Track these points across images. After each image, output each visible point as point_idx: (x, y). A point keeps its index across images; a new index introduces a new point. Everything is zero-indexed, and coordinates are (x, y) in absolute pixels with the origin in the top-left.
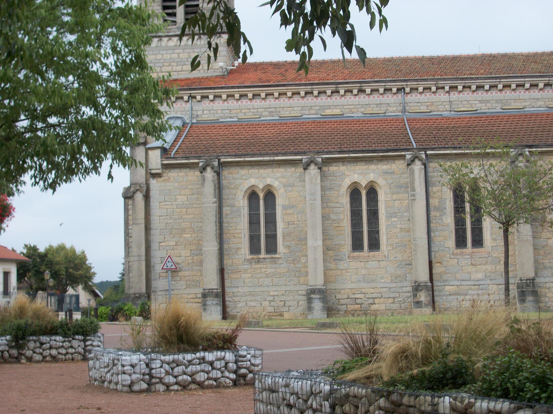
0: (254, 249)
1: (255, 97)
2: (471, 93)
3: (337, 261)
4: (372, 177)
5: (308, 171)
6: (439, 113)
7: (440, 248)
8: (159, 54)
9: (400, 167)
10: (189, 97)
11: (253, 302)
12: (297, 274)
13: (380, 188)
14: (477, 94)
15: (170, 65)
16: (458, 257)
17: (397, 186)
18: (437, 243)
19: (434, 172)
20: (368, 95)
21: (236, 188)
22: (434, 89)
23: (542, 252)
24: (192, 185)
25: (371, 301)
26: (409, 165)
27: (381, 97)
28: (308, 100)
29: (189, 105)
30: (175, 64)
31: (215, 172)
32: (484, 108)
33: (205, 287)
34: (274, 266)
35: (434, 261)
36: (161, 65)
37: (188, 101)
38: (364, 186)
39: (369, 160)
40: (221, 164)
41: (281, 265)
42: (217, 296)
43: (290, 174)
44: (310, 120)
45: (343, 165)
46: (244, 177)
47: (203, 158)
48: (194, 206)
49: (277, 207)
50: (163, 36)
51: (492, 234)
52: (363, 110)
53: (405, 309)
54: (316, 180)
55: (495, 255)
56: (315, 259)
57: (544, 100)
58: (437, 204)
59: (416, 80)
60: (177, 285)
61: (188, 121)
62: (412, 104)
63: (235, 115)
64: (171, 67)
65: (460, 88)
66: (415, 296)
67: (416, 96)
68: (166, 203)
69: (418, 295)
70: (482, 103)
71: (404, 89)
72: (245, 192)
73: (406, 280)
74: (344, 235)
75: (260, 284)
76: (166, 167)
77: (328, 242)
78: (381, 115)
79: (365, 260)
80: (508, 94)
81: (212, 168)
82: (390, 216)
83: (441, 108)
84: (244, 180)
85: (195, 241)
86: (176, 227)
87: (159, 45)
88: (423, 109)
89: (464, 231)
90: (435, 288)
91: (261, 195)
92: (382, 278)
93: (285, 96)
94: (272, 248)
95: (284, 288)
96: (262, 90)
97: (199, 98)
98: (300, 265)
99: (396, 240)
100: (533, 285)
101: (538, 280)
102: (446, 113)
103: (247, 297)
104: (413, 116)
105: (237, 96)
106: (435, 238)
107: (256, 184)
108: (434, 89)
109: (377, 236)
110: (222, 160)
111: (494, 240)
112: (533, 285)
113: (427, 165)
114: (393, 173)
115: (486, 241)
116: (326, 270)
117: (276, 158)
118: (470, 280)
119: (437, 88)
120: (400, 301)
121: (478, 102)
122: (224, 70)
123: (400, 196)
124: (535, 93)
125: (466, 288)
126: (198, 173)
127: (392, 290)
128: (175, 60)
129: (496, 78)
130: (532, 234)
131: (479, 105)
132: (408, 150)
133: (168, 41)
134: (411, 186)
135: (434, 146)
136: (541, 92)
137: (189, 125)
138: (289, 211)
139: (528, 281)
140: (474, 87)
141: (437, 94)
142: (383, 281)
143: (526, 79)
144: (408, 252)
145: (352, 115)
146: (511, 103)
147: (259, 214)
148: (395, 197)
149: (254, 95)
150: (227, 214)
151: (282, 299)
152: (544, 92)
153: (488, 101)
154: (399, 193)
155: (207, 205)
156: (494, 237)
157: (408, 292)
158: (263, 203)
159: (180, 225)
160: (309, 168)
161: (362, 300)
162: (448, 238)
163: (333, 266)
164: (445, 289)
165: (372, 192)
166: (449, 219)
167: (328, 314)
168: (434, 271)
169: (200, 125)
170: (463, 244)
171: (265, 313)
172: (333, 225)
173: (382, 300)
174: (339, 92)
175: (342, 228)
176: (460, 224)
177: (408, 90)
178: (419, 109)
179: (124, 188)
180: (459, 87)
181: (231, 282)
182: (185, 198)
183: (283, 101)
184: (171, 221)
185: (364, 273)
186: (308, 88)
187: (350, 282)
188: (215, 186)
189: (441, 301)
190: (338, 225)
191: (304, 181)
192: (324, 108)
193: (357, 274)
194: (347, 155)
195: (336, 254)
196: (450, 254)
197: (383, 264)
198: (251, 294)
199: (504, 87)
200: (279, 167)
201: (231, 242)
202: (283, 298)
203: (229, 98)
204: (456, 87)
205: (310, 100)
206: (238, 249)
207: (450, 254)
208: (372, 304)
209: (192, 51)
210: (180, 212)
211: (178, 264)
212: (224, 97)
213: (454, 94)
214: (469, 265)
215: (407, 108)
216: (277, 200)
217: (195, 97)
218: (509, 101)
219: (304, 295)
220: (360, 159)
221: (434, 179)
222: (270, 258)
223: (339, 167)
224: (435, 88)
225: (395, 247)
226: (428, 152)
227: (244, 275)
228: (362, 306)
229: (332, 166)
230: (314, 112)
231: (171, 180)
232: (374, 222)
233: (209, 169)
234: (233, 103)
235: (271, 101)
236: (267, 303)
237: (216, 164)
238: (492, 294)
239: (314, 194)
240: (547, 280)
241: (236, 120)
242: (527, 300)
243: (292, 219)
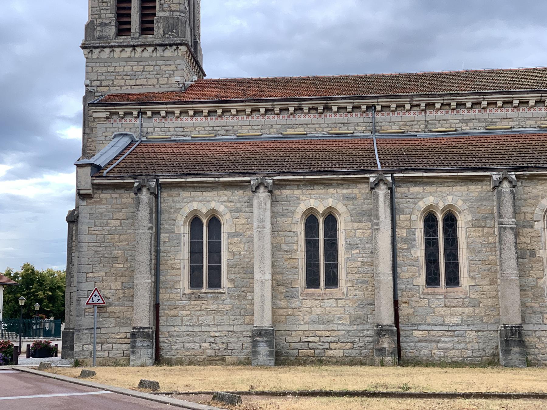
0: (195, 283)
1: (211, 114)
2: (450, 112)
3: (288, 298)
4: (330, 202)
5: (256, 194)
6: (413, 134)
7: (408, 286)
8: (111, 66)
9: (363, 191)
10: (139, 113)
11: (190, 344)
12: (242, 312)
13: (340, 215)
14: (458, 112)
15: (122, 79)
16: (429, 297)
17: (359, 213)
18: (405, 280)
19: (402, 198)
20: (334, 113)
21: (177, 212)
22: (408, 106)
23: (530, 294)
24: (127, 208)
25: (327, 346)
26: (372, 189)
27: (349, 115)
28: (268, 118)
29: (138, 121)
30: (129, 77)
31: (151, 194)
32: (464, 128)
33: (134, 325)
34: (215, 302)
35: (400, 300)
36: (113, 78)
37: (138, 117)
38: (321, 212)
39: (327, 184)
40: (159, 185)
41: (225, 302)
42: (147, 336)
43: (237, 198)
44: (270, 140)
45: (298, 189)
46: (185, 200)
47: (140, 177)
48: (128, 232)
49: (222, 235)
50: (115, 46)
51: (469, 271)
52: (327, 129)
53: (366, 356)
54: (266, 205)
55: (473, 296)
56: (262, 295)
57: (535, 119)
58: (405, 235)
59: (388, 97)
60: (104, 322)
61: (137, 139)
62: (383, 124)
63: (189, 133)
64: (124, 81)
65: (438, 105)
67: (388, 114)
68: (97, 228)
69: (380, 341)
70: (462, 123)
71: (375, 107)
72: (187, 217)
73: (367, 322)
74: (296, 268)
75: (200, 322)
76: (97, 187)
77: (279, 277)
78: (348, 135)
79: (320, 298)
80: (493, 113)
81: (148, 189)
82: (350, 247)
83: (416, 128)
84: (187, 204)
85: (127, 272)
86: (106, 255)
87: (112, 56)
88: (396, 129)
89: (437, 266)
90: (401, 333)
91: (205, 221)
92: (340, 319)
93: (243, 113)
94: (215, 282)
95: (227, 328)
96: (219, 107)
97: (149, 113)
98: (246, 302)
99: (357, 276)
100: (520, 333)
101: (525, 327)
102: (421, 133)
103: (185, 338)
104: (385, 137)
105: (191, 112)
106: (401, 275)
107: (199, 208)
108: (408, 106)
109: (335, 270)
110: (161, 180)
111: (473, 278)
112: (520, 333)
113: (394, 190)
114: (354, 198)
115: (462, 279)
116: (275, 308)
117: (222, 179)
118: (442, 325)
119: (412, 106)
120: (360, 347)
121: (458, 121)
122: (181, 85)
123: (362, 225)
124: (524, 112)
125: (438, 334)
126: (133, 195)
127: (351, 334)
128: (129, 73)
129: (480, 94)
130: (518, 272)
131: (460, 125)
132: (371, 172)
133: (121, 52)
134: (372, 215)
135: (402, 168)
136: (532, 110)
137: (137, 143)
138: (235, 240)
139: (514, 328)
140: (454, 105)
141: (412, 113)
142: (341, 322)
143: (515, 96)
144: (370, 290)
145: (317, 135)
146: (496, 122)
147: (202, 242)
148: (356, 225)
149: (209, 112)
150: (165, 242)
151: (224, 341)
152: (535, 110)
153: (470, 120)
154: (361, 221)
155: (141, 231)
156: (472, 274)
157: (370, 337)
158: (206, 230)
159: (111, 254)
160: (258, 190)
161: (316, 345)
162: (417, 275)
163: (283, 304)
164: (414, 335)
165: (331, 220)
166: (419, 253)
167: (276, 360)
168: (400, 313)
169: (149, 144)
170: (454, 282)
171: (204, 356)
172: (284, 256)
173: (339, 345)
174: (302, 109)
175: (294, 260)
176: (432, 259)
177: (379, 108)
178: (391, 129)
179: (69, 211)
180: (436, 104)
181: (167, 320)
182: (118, 222)
183: (242, 120)
184: (101, 249)
185: (319, 313)
186: (269, 105)
187: (302, 323)
188: (151, 209)
189: (408, 348)
190: (290, 256)
191: (252, 206)
193: (311, 313)
194: (302, 177)
195: (287, 290)
196: (419, 293)
197: (341, 303)
198: (189, 334)
199: (488, 104)
200: (225, 190)
201: (168, 274)
202: (225, 340)
203: (183, 115)
204: (434, 105)
205: (270, 119)
206: (177, 281)
207: (419, 293)
208: (327, 349)
209: (147, 64)
210: (112, 239)
211: (107, 298)
212: (177, 113)
213: (431, 113)
214: (442, 307)
215: (378, 128)
216: (222, 226)
217: (145, 113)
218: (494, 120)
219: (250, 337)
220: (316, 182)
221: (401, 206)
222: (212, 293)
223: (293, 190)
224: (409, 105)
225: (355, 283)
226: (395, 175)
227: (182, 312)
228: (316, 351)
229: (285, 189)
230: (275, 131)
231: (103, 202)
232: (333, 254)
233: (145, 190)
234: (186, 120)
235: (228, 120)
236: (206, 345)
237: (153, 184)
238: (469, 342)
239: (263, 221)
240: (536, 327)
241: (190, 138)
242: (512, 352)
243: (238, 249)
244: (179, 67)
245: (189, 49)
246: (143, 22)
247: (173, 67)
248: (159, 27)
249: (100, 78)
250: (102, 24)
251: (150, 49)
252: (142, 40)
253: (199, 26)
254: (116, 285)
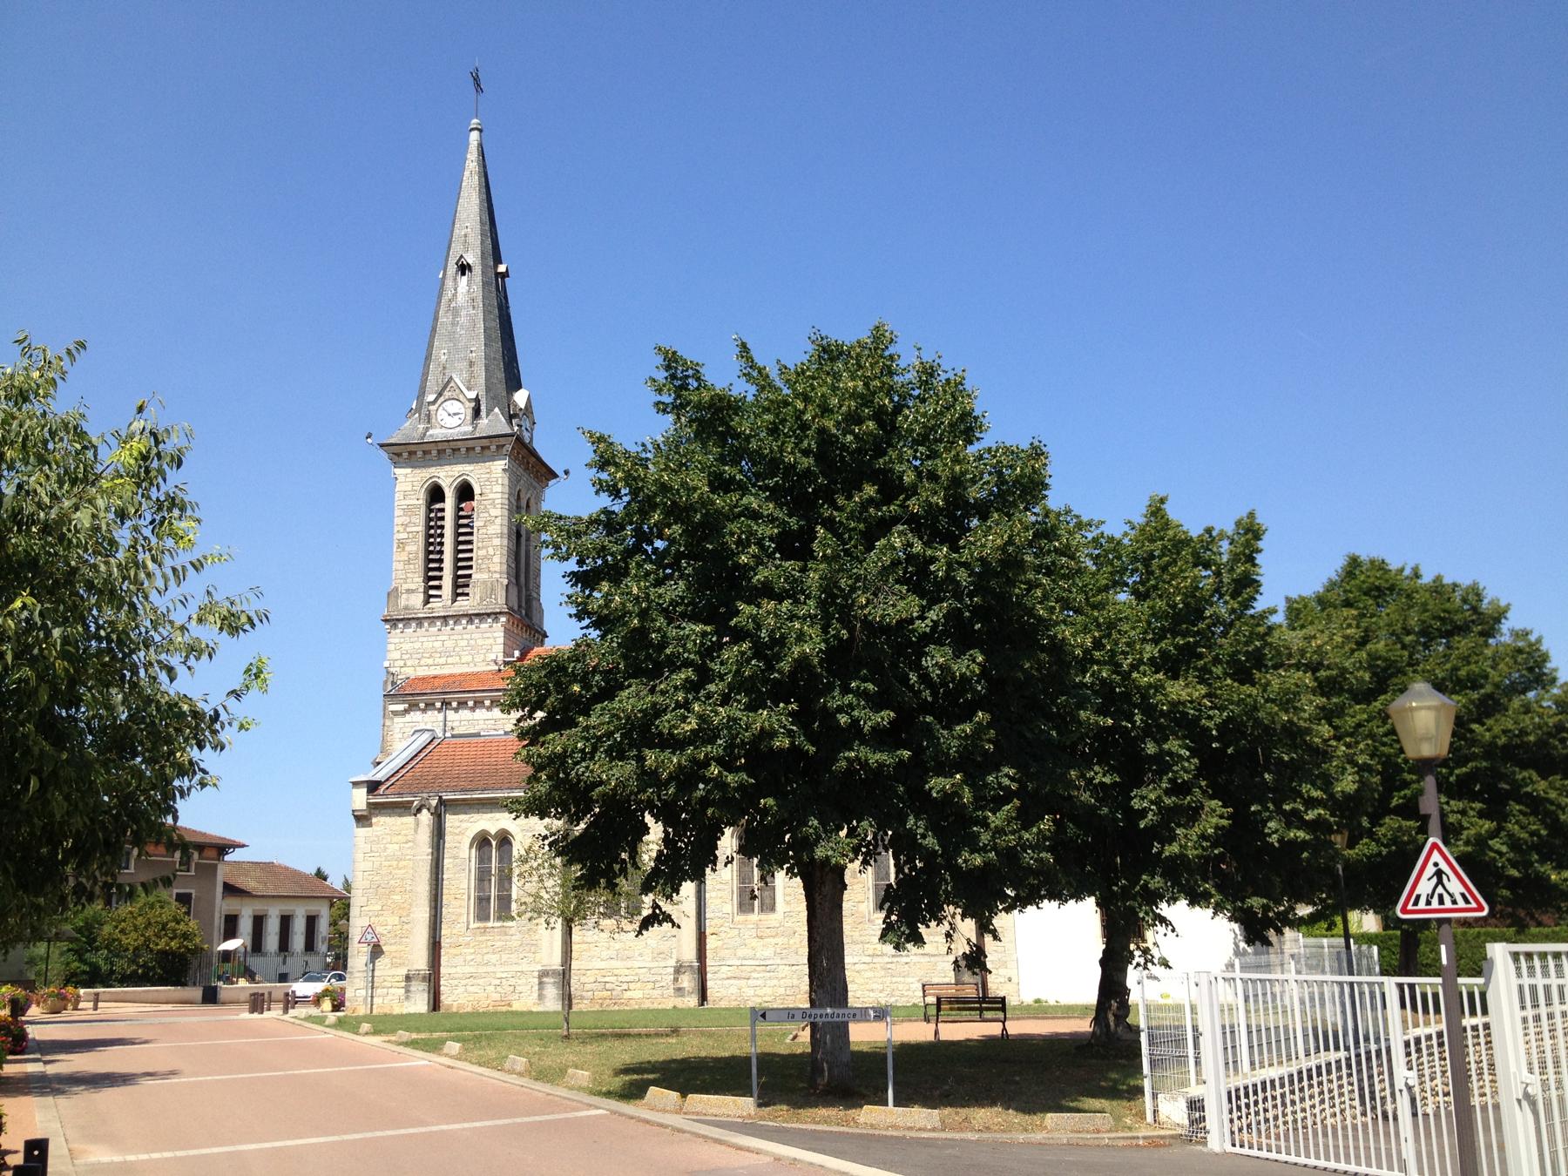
25: (625, 986)
40: (441, 801)
66: (676, 980)
111: (788, 903)
202: (512, 982)
236: (492, 988)
246: (456, 586)
250: (409, 591)
253: (538, 575)
254: (394, 920)
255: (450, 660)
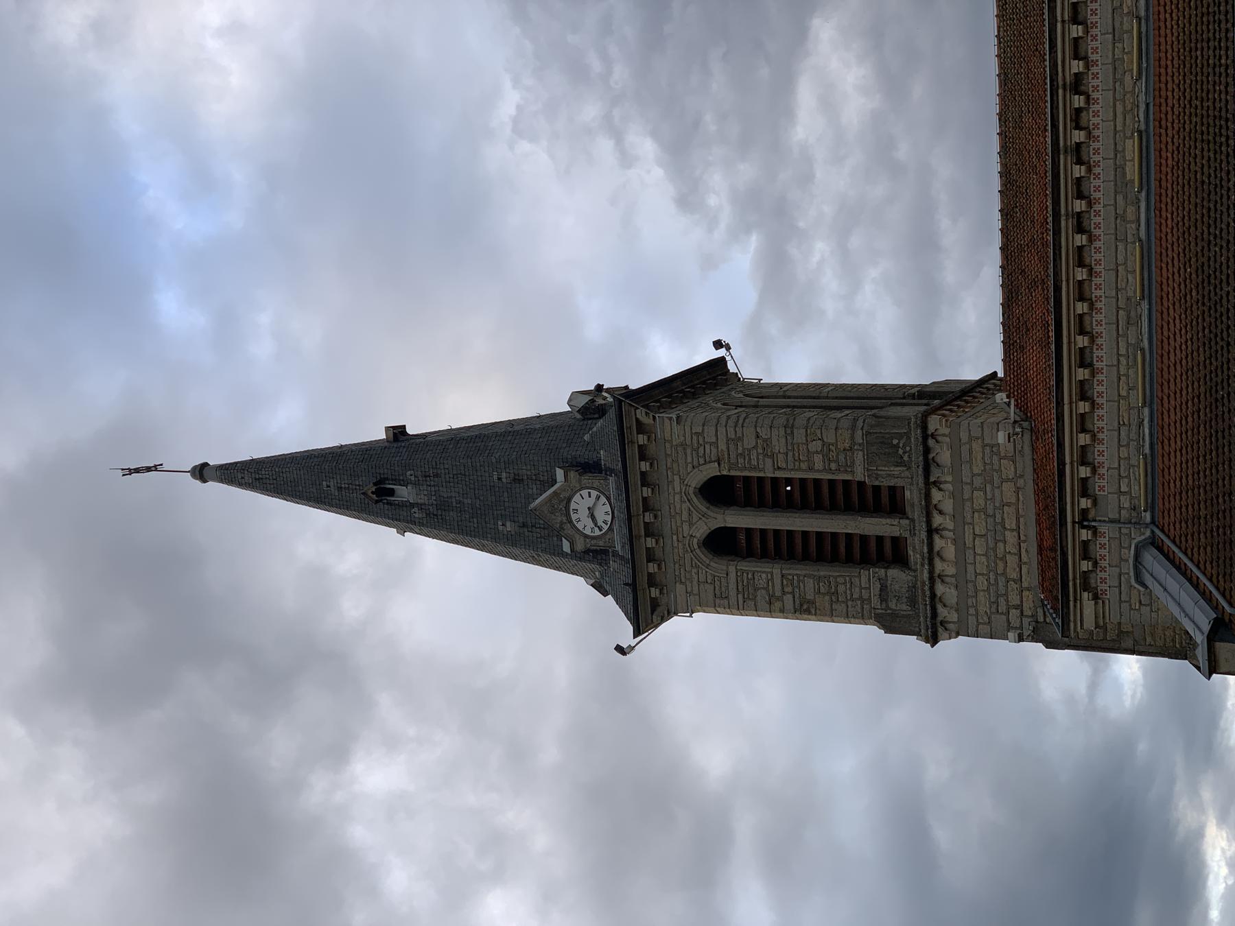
15: (1003, 559)
29: (1103, 528)
37: (1095, 531)
97: (1085, 503)
145: (1142, 107)
192: (1121, 184)
217: (1084, 512)
235: (1101, 322)
244: (976, 432)
245: (934, 411)
247: (976, 446)
248: (888, 476)
249: (1003, 608)
251: (936, 495)
252: (917, 513)
255: (1010, 523)
